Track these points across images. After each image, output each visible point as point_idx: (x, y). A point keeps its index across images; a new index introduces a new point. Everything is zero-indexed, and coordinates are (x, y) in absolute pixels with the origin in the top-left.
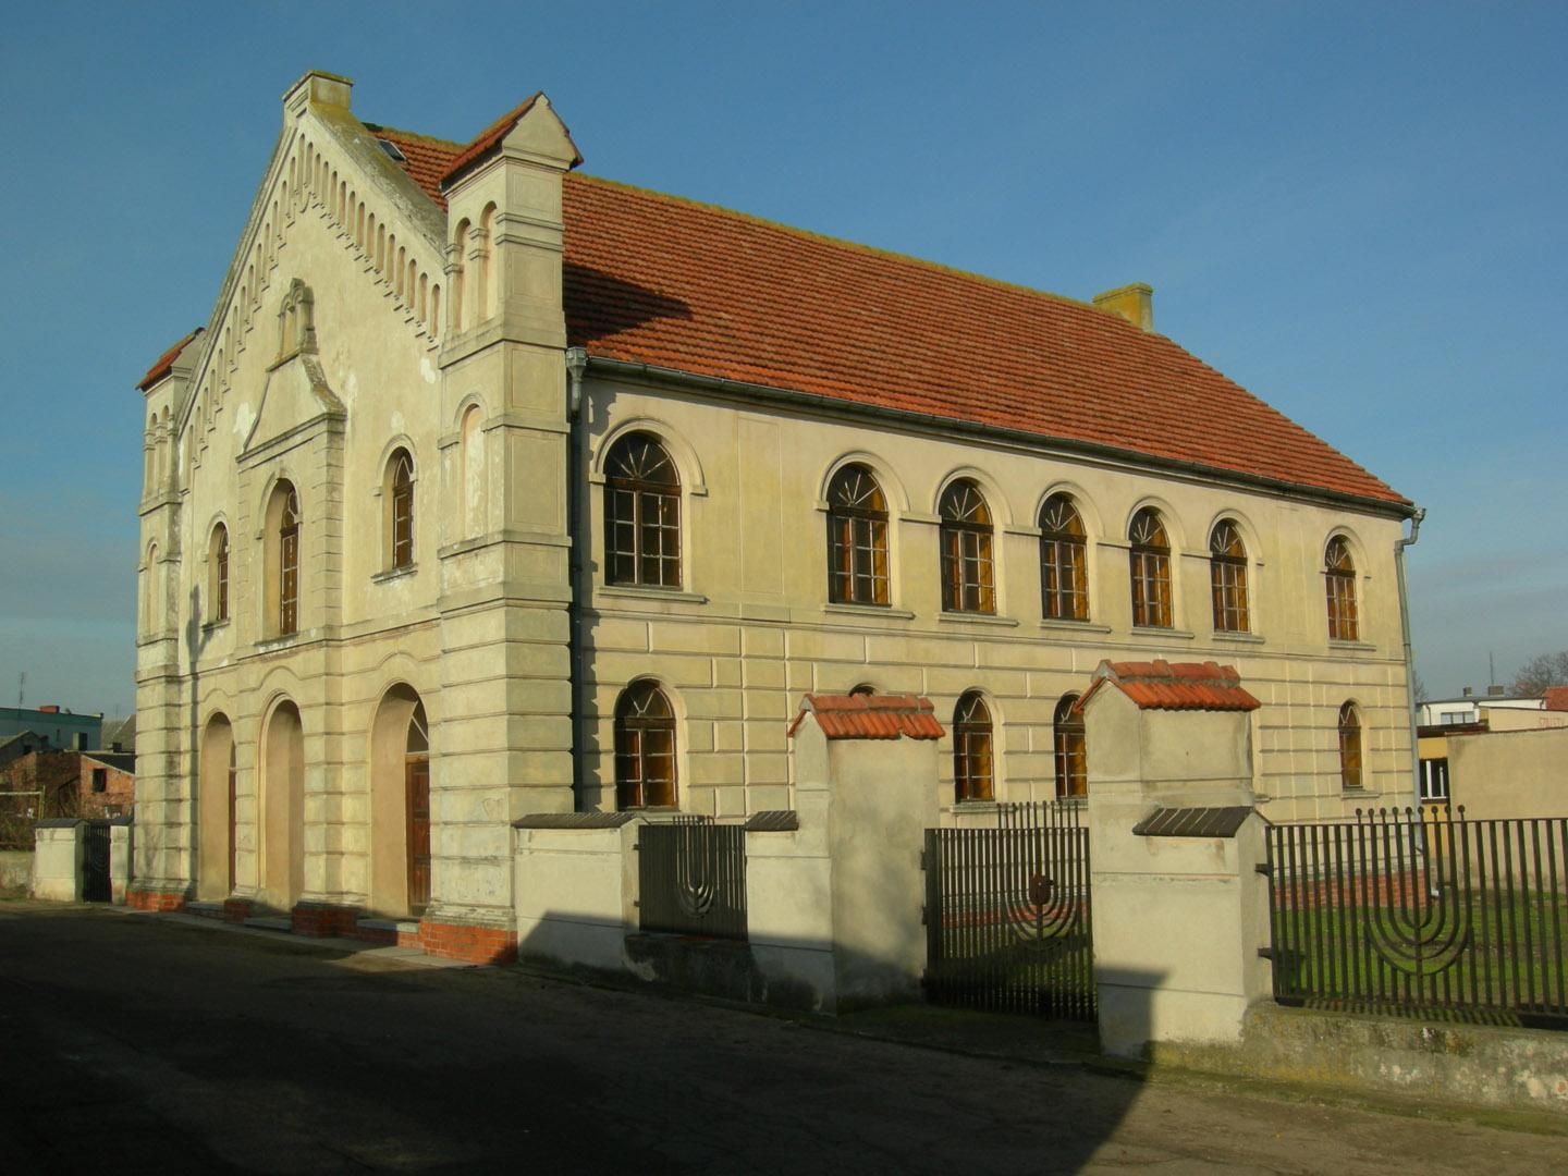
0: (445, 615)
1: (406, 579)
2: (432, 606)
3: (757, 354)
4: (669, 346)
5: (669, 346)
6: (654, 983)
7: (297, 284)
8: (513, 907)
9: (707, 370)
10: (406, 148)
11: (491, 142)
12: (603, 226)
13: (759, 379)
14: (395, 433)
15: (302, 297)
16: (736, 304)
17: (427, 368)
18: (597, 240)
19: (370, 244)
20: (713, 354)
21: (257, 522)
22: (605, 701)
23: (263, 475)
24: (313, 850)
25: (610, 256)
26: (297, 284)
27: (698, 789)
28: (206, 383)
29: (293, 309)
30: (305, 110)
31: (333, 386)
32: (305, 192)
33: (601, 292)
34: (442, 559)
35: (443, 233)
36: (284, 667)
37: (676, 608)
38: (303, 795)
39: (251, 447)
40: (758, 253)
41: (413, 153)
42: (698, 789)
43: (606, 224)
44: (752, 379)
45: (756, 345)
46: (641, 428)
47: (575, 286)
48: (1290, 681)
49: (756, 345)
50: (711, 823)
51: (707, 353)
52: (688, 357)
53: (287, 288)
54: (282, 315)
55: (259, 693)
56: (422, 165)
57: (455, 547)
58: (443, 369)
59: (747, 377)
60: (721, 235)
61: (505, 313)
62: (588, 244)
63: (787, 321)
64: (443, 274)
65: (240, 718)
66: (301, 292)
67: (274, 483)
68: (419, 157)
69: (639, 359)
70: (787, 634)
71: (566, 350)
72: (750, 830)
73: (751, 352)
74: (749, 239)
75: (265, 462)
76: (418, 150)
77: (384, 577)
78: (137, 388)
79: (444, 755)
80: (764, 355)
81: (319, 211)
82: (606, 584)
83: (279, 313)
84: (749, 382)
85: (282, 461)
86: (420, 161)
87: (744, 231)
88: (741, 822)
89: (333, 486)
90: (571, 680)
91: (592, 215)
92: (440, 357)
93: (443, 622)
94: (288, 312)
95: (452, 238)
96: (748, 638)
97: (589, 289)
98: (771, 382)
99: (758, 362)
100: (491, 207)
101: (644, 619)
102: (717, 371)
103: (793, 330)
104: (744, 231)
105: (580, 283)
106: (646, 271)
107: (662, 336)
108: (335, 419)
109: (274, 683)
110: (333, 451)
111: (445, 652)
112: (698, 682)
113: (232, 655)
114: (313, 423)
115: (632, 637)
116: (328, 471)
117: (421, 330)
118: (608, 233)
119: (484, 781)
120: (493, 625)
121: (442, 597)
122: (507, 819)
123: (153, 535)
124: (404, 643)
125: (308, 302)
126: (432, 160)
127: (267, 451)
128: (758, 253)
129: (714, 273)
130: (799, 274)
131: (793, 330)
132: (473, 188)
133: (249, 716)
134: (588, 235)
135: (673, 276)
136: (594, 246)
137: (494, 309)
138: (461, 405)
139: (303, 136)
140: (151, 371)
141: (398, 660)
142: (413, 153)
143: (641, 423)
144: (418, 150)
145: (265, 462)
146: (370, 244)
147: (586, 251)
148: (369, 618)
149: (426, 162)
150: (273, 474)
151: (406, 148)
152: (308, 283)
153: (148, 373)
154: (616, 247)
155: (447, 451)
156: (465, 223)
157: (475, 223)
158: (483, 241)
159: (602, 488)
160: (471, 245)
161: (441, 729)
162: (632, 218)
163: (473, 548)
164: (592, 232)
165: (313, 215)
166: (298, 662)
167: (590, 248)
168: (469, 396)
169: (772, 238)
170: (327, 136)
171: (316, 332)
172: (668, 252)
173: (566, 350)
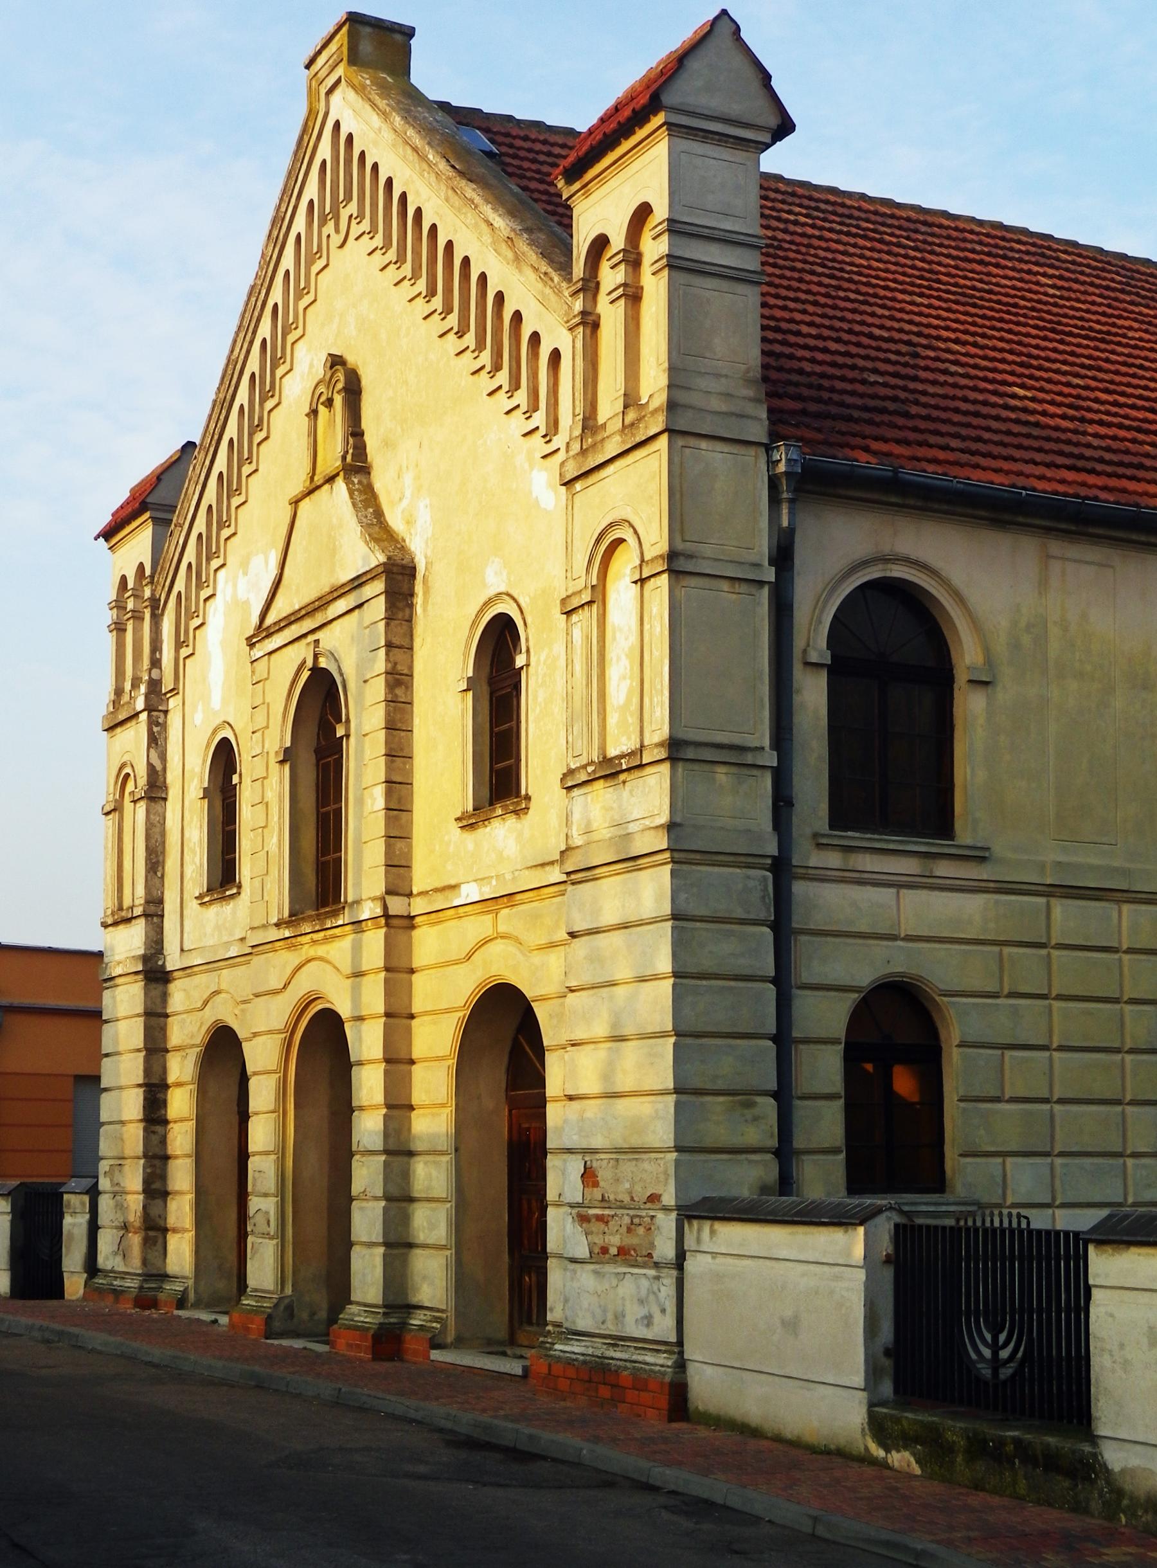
0: (573, 877)
1: (511, 820)
2: (552, 863)
3: (1076, 451)
4: (932, 439)
5: (932, 439)
6: (921, 1476)
7: (336, 361)
8: (680, 1343)
9: (998, 478)
10: (500, 139)
11: (644, 100)
12: (816, 256)
13: (1083, 492)
14: (492, 592)
15: (346, 385)
16: (1038, 373)
17: (543, 484)
18: (808, 277)
19: (448, 290)
20: (1004, 451)
21: (279, 735)
22: (825, 1016)
23: (287, 665)
24: (364, 1239)
25: (830, 302)
26: (336, 361)
27: (997, 1169)
28: (200, 526)
29: (329, 403)
30: (339, 81)
31: (395, 520)
32: (344, 214)
33: (820, 356)
34: (569, 789)
35: (565, 268)
36: (321, 959)
37: (944, 869)
38: (351, 1155)
39: (270, 619)
40: (1066, 294)
41: (511, 146)
42: (997, 1169)
43: (822, 253)
44: (1071, 491)
45: (1074, 438)
46: (888, 574)
47: (778, 348)
48: (1130, 951)
49: (1074, 438)
50: (1024, 1225)
51: (997, 450)
52: (965, 457)
53: (319, 370)
54: (314, 413)
55: (280, 997)
56: (526, 165)
57: (590, 769)
58: (568, 484)
59: (1061, 488)
60: (1006, 267)
61: (670, 386)
62: (795, 284)
63: (1122, 400)
64: (566, 332)
65: (255, 1035)
66: (341, 376)
67: (306, 674)
68: (522, 153)
69: (885, 460)
70: (1126, 908)
71: (768, 449)
72: (1100, 1243)
73: (1068, 449)
74: (1051, 271)
75: (290, 643)
76: (519, 143)
77: (471, 821)
78: (96, 539)
79: (571, 1098)
80: (1088, 453)
81: (367, 244)
82: (831, 827)
83: (307, 410)
84: (1065, 495)
85: (317, 642)
86: (522, 159)
87: (1042, 260)
88: (1084, 1220)
89: (399, 681)
90: (775, 981)
91: (798, 239)
92: (562, 464)
93: (570, 888)
94: (321, 408)
95: (579, 269)
96: (1065, 918)
97: (800, 353)
98: (1103, 495)
99: (1080, 463)
100: (643, 212)
101: (900, 884)
102: (1013, 479)
103: (1134, 413)
104: (1042, 260)
105: (784, 343)
106: (889, 323)
107: (923, 425)
108: (399, 579)
109: (303, 985)
110: (393, 623)
111: (573, 935)
112: (977, 985)
113: (243, 939)
114: (358, 583)
115: (884, 913)
116: (387, 654)
117: (531, 425)
118: (824, 266)
119: (635, 1142)
120: (653, 890)
121: (569, 849)
122: (673, 1203)
123: (126, 758)
124: (507, 920)
125: (353, 391)
126: (542, 158)
127: (293, 627)
128: (1066, 294)
129: (999, 325)
130: (1136, 325)
131: (1134, 413)
132: (612, 183)
133: (270, 1032)
134: (793, 269)
135: (934, 332)
136: (804, 287)
137: (654, 382)
138: (598, 541)
139: (337, 125)
140: (117, 511)
141: (497, 947)
142: (511, 146)
143: (890, 566)
144: (519, 143)
145: (290, 643)
146: (448, 290)
147: (792, 294)
148: (453, 882)
149: (534, 161)
150: (304, 662)
151: (500, 139)
152: (351, 359)
153: (113, 515)
154: (839, 288)
155: (575, 618)
156: (600, 243)
157: (618, 242)
158: (630, 270)
159: (824, 675)
160: (611, 277)
161: (566, 1056)
162: (861, 242)
163: (611, 770)
164: (799, 265)
165: (358, 249)
166: (340, 949)
167: (798, 290)
168: (611, 525)
169: (1088, 271)
170: (375, 120)
171: (367, 438)
172: (921, 295)
173: (768, 449)
